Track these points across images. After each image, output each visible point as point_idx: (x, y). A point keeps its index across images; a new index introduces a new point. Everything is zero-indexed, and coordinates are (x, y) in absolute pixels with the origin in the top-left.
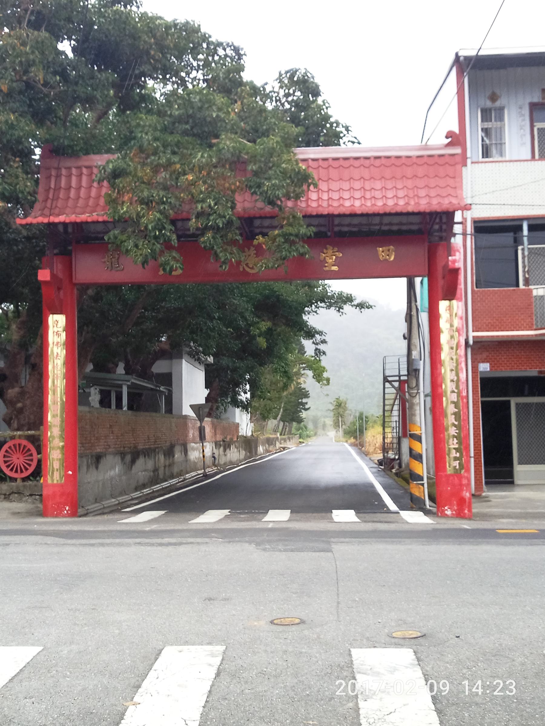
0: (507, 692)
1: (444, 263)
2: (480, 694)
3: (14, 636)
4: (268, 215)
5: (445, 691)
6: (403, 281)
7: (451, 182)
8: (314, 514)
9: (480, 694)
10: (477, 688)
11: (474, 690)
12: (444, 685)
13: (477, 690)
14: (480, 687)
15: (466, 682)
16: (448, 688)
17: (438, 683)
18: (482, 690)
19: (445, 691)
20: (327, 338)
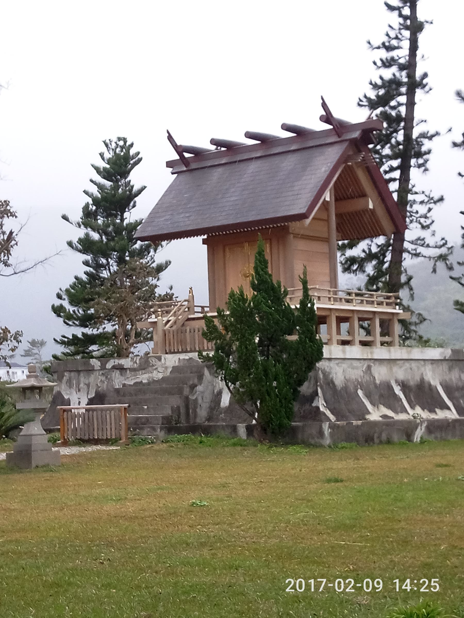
0: (432, 589)
1: (230, 290)
2: (409, 590)
3: (3, 451)
4: (327, 361)
5: (379, 588)
6: (208, 305)
7: (361, 212)
8: (307, 208)
9: (409, 590)
10: (406, 586)
11: (403, 587)
12: (378, 583)
13: (406, 588)
14: (409, 585)
15: (397, 581)
16: (381, 585)
17: (373, 583)
18: (411, 588)
19: (379, 588)
20: (433, 219)
